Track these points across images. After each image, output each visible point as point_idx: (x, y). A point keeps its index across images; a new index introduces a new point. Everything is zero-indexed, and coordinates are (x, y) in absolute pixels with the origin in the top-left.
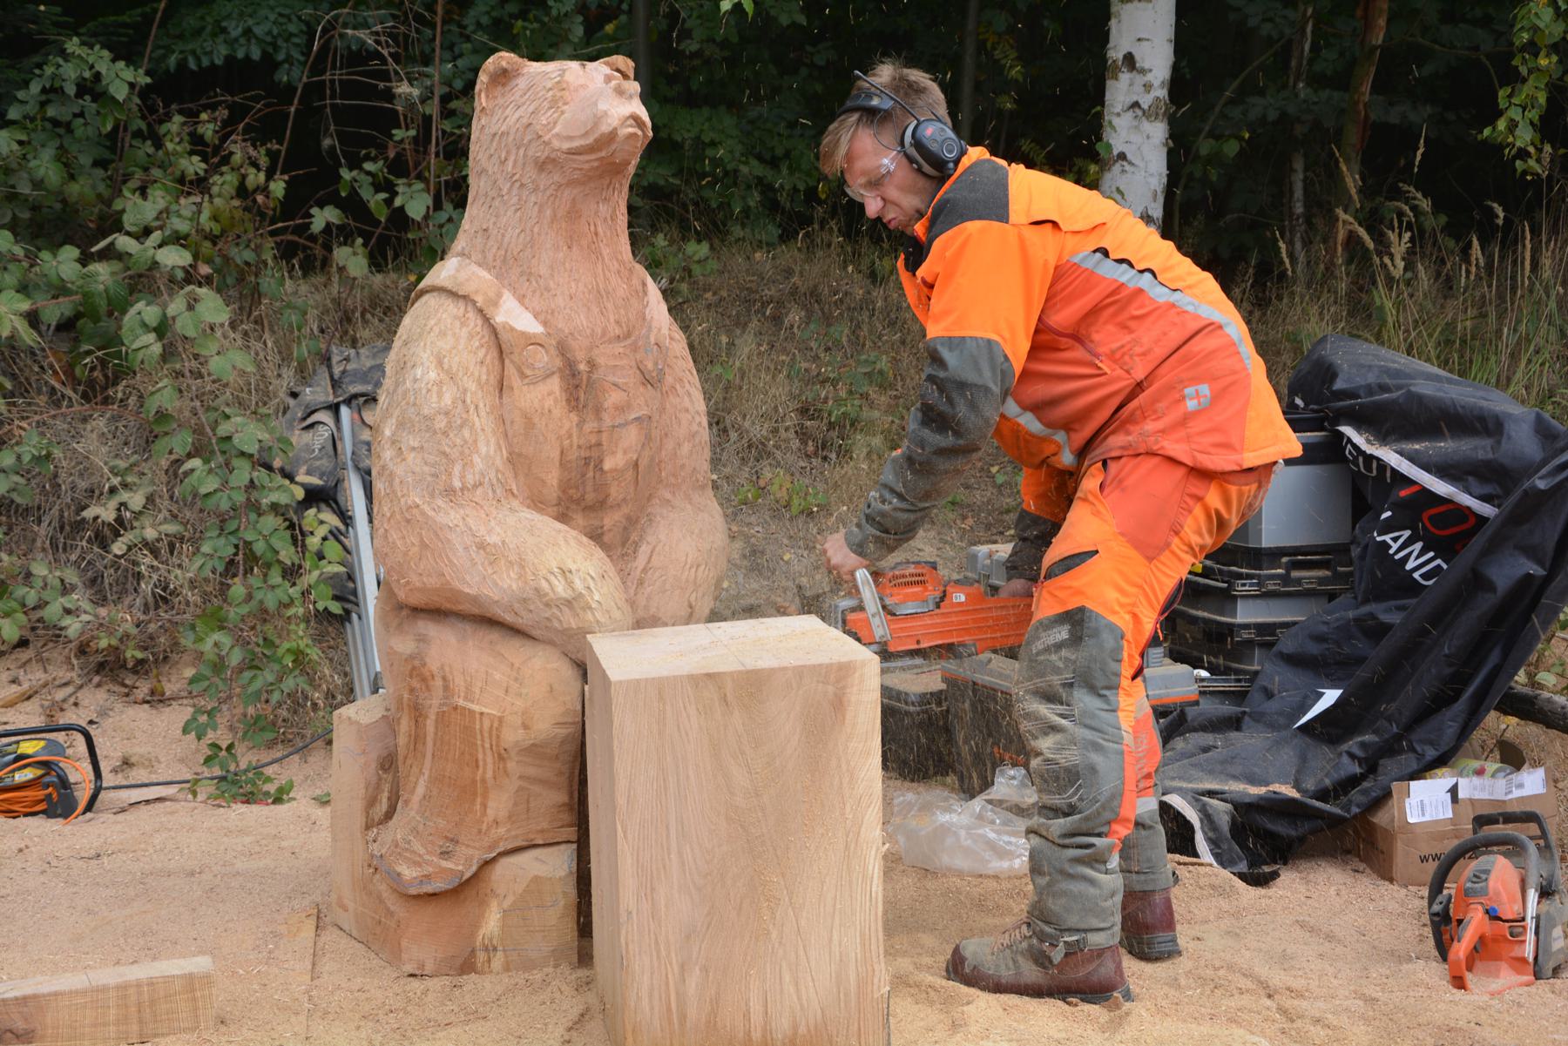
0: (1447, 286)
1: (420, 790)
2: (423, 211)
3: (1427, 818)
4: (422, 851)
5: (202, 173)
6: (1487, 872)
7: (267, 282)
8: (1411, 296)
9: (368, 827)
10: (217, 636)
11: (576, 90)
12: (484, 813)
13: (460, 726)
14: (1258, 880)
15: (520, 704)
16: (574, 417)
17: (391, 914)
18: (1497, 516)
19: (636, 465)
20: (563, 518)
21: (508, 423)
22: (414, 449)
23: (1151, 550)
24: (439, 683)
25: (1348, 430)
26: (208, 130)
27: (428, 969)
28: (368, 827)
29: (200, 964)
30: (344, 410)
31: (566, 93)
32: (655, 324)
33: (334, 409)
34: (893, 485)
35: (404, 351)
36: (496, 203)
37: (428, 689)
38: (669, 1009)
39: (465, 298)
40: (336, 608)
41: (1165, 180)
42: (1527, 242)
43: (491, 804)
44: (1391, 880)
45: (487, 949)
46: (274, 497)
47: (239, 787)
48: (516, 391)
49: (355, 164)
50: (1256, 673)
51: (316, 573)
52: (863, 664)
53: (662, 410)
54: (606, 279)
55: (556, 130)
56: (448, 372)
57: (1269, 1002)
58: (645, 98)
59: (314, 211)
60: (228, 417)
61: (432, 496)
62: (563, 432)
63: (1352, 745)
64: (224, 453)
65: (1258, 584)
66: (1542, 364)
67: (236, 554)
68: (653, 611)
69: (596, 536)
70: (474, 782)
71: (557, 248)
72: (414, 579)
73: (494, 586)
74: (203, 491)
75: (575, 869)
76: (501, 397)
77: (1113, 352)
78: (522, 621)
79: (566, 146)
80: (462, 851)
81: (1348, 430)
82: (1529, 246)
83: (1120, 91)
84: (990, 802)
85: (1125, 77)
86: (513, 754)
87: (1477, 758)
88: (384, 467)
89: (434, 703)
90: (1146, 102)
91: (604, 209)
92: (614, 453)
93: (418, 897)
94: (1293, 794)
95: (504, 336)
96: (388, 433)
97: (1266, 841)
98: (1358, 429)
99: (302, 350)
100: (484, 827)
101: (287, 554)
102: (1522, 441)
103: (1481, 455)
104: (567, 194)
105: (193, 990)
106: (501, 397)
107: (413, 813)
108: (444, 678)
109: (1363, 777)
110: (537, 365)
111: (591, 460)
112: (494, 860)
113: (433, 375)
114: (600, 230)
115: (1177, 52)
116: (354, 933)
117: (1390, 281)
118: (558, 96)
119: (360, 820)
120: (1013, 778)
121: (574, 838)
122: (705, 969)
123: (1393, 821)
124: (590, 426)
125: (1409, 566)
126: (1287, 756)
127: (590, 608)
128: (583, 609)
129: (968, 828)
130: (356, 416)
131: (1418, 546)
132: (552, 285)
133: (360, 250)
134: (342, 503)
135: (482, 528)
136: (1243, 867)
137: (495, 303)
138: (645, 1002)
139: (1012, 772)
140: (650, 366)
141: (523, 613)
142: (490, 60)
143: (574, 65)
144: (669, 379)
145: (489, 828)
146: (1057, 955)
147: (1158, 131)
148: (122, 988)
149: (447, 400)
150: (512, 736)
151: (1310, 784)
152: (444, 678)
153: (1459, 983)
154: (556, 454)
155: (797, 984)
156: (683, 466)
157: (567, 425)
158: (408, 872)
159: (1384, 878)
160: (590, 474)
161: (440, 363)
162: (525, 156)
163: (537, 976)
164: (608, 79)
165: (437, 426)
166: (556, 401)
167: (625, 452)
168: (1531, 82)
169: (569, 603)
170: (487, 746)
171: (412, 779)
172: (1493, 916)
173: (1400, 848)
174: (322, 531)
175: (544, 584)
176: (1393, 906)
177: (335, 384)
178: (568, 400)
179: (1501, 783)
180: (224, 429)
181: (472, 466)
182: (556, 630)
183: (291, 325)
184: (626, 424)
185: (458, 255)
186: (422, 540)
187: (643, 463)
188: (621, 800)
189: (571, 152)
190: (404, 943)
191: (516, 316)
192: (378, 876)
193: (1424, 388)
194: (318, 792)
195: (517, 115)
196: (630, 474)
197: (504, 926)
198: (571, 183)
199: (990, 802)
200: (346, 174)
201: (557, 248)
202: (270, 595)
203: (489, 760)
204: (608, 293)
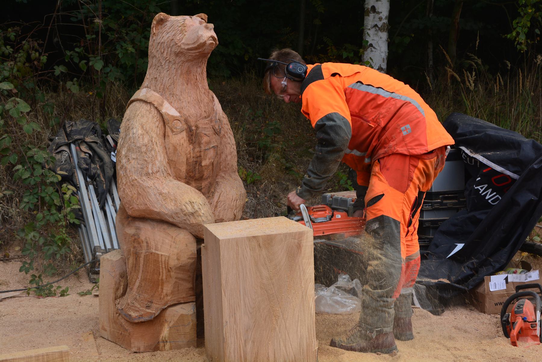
0: (489, 93)
1: (137, 284)
3: (497, 289)
4: (139, 306)
5: (11, 53)
6: (523, 305)
7: (39, 95)
8: (477, 97)
9: (116, 299)
10: (32, 234)
11: (189, 27)
12: (162, 292)
13: (153, 259)
14: (435, 313)
15: (176, 251)
16: (191, 146)
17: (126, 330)
18: (519, 179)
19: (213, 164)
20: (188, 183)
21: (167, 149)
22: (134, 159)
23: (403, 189)
25: (463, 148)
26: (12, 35)
27: (142, 349)
28: (116, 299)
29: (64, 348)
30: (73, 146)
31: (186, 28)
32: (218, 112)
33: (69, 145)
34: (312, 170)
35: (128, 123)
36: (160, 68)
38: (241, 357)
39: (150, 103)
40: (77, 222)
41: (387, 54)
42: (521, 76)
43: (164, 288)
44: (485, 313)
45: (163, 342)
46: (52, 179)
47: (42, 292)
49: (72, 49)
50: (432, 238)
51: (69, 209)
52: (308, 232)
53: (221, 143)
54: (201, 96)
55: (183, 41)
56: (145, 130)
57: (448, 352)
58: (215, 30)
59: (56, 67)
60: (30, 149)
62: (187, 152)
63: (468, 263)
64: (30, 163)
65: (431, 206)
66: (527, 123)
67: (38, 202)
68: (221, 217)
69: (200, 189)
71: (183, 85)
73: (165, 208)
74: (24, 177)
75: (195, 311)
76: (165, 139)
77: (373, 119)
78: (176, 220)
79: (186, 47)
80: (154, 306)
81: (463, 148)
82: (521, 78)
83: (370, 20)
84: (337, 287)
85: (372, 15)
86: (173, 269)
87: (513, 267)
88: (123, 166)
90: (380, 24)
91: (199, 70)
93: (138, 323)
94: (448, 282)
95: (165, 117)
96: (123, 153)
97: (442, 298)
98: (467, 147)
99: (52, 122)
100: (162, 297)
101: (57, 202)
102: (528, 151)
103: (513, 156)
105: (62, 357)
106: (165, 139)
107: (134, 293)
108: (147, 243)
109: (472, 276)
110: (178, 127)
111: (198, 162)
112: (166, 309)
113: (140, 132)
114: (198, 78)
115: (390, 6)
116: (110, 339)
117: (468, 90)
118: (183, 29)
119: (112, 296)
120: (345, 278)
121: (194, 300)
122: (253, 342)
123: (485, 291)
124: (197, 149)
125: (487, 198)
126: (444, 270)
127: (200, 216)
128: (198, 216)
129: (331, 296)
130: (78, 148)
131: (490, 190)
132: (181, 98)
134: (75, 182)
135: (161, 187)
136: (431, 308)
137: (162, 105)
138: (232, 354)
139: (344, 276)
140: (217, 127)
141: (176, 218)
142: (157, 16)
143: (187, 17)
144: (223, 132)
146: (374, 335)
147: (384, 35)
148: (37, 356)
149: (146, 141)
150: (173, 263)
151: (453, 278)
152: (147, 243)
153: (514, 344)
154: (185, 160)
155: (285, 347)
156: (228, 164)
157: (189, 149)
158: (134, 314)
159: (481, 312)
160: (197, 167)
161: (142, 127)
162: (171, 51)
163: (183, 350)
164: (201, 23)
165: (143, 150)
166: (185, 140)
167: (209, 159)
168: (525, 18)
169: (192, 214)
170: (164, 267)
172: (524, 320)
173: (487, 300)
174: (69, 193)
175: (184, 207)
176: (486, 321)
177: (68, 135)
178: (189, 140)
179: (523, 276)
180: (30, 153)
182: (188, 224)
183: (48, 112)
184: (210, 149)
185: (145, 87)
186: (138, 192)
187: (215, 163)
188: (223, 282)
189: (188, 49)
190: (132, 341)
191: (169, 110)
192: (120, 317)
193: (491, 132)
194: (79, 291)
195: (167, 36)
196: (211, 167)
197: (170, 333)
198: (188, 61)
199: (337, 287)
200: (68, 53)
201: (183, 85)
202: (52, 217)
203: (164, 272)
204: (201, 101)
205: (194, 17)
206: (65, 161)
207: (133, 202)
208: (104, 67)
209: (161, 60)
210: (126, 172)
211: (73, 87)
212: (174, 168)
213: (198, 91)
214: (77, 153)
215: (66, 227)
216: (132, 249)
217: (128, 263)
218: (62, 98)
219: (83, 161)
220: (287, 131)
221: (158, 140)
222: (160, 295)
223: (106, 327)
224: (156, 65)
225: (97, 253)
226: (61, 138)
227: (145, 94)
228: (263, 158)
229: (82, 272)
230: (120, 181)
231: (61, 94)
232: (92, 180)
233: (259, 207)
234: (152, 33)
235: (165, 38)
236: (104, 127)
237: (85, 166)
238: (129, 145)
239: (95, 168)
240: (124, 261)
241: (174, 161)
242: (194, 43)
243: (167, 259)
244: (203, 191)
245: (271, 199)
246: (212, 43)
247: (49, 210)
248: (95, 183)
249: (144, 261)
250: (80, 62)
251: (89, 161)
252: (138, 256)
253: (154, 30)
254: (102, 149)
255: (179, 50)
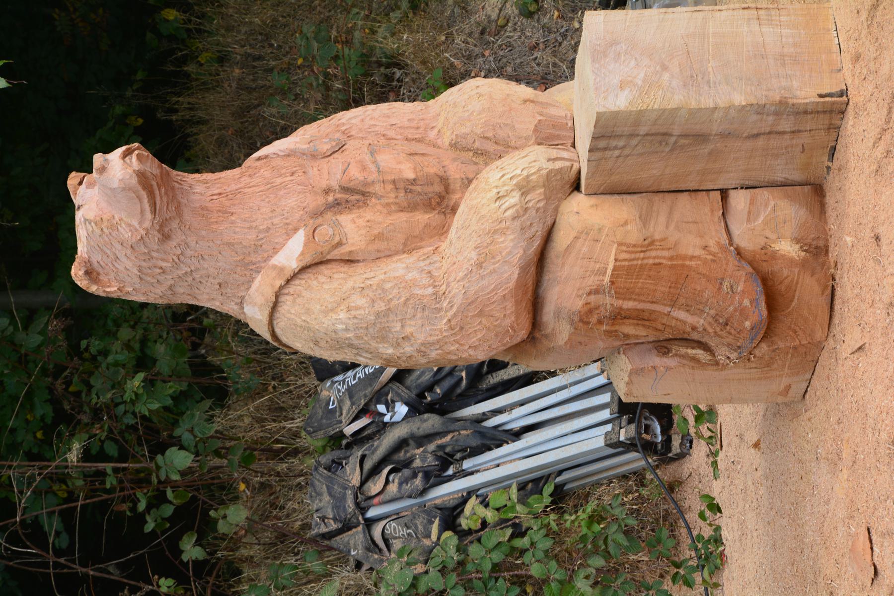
1: (682, 315)
2: (183, 453)
11: (101, 210)
20: (454, 210)
21: (379, 255)
24: (592, 298)
30: (371, 513)
31: (105, 217)
33: (370, 523)
35: (322, 344)
36: (196, 276)
37: (597, 308)
39: (277, 295)
40: (549, 489)
43: (690, 252)
47: (711, 555)
48: (353, 249)
51: (519, 508)
56: (339, 305)
58: (108, 150)
61: (439, 310)
62: (385, 211)
70: (672, 267)
72: (508, 322)
73: (513, 251)
76: (358, 261)
78: (539, 231)
79: (149, 215)
88: (419, 351)
89: (608, 302)
91: (199, 189)
92: (401, 171)
95: (308, 260)
96: (390, 351)
99: (315, 565)
100: (709, 257)
104: (187, 216)
108: (589, 294)
113: (342, 315)
114: (216, 192)
116: (808, 376)
119: (711, 373)
124: (378, 188)
127: (528, 176)
128: (528, 182)
130: (376, 500)
133: (221, 512)
134: (456, 502)
137: (282, 269)
141: (533, 230)
142: (79, 283)
143: (79, 216)
144: (338, 135)
145: (711, 253)
154: (403, 217)
157: (379, 207)
160: (418, 188)
162: (157, 251)
164: (91, 185)
166: (360, 217)
170: (642, 255)
171: (673, 323)
174: (482, 512)
177: (347, 527)
178: (359, 207)
181: (414, 280)
184: (375, 162)
189: (154, 211)
191: (291, 253)
195: (124, 259)
203: (653, 253)
205: (77, 201)
206: (408, 528)
207: (499, 326)
208: (182, 448)
209: (180, 273)
210: (433, 344)
211: (234, 517)
212: (422, 239)
213: (246, 190)
214: (391, 502)
215: (561, 511)
216: (604, 327)
217: (637, 337)
218: (255, 551)
219: (407, 487)
220: (320, 13)
221: (357, 277)
222: (705, 262)
223: (782, 387)
224: (190, 286)
225: (622, 438)
226: (355, 540)
227: (257, 309)
228: (388, 66)
229: (667, 473)
230: (454, 357)
231: (244, 552)
232: (452, 463)
233: (509, 69)
234: (119, 294)
235: (129, 264)
236: (324, 447)
237: (418, 482)
238: (374, 338)
239: (422, 457)
240: (628, 345)
241: (407, 239)
242: (139, 198)
243: (624, 248)
244: (471, 176)
245: (488, 43)
246: (138, 156)
247: (523, 552)
248: (458, 456)
249: (630, 299)
250: (171, 503)
251: (406, 472)
252: (619, 313)
253: (112, 289)
254: (376, 444)
255: (156, 233)
